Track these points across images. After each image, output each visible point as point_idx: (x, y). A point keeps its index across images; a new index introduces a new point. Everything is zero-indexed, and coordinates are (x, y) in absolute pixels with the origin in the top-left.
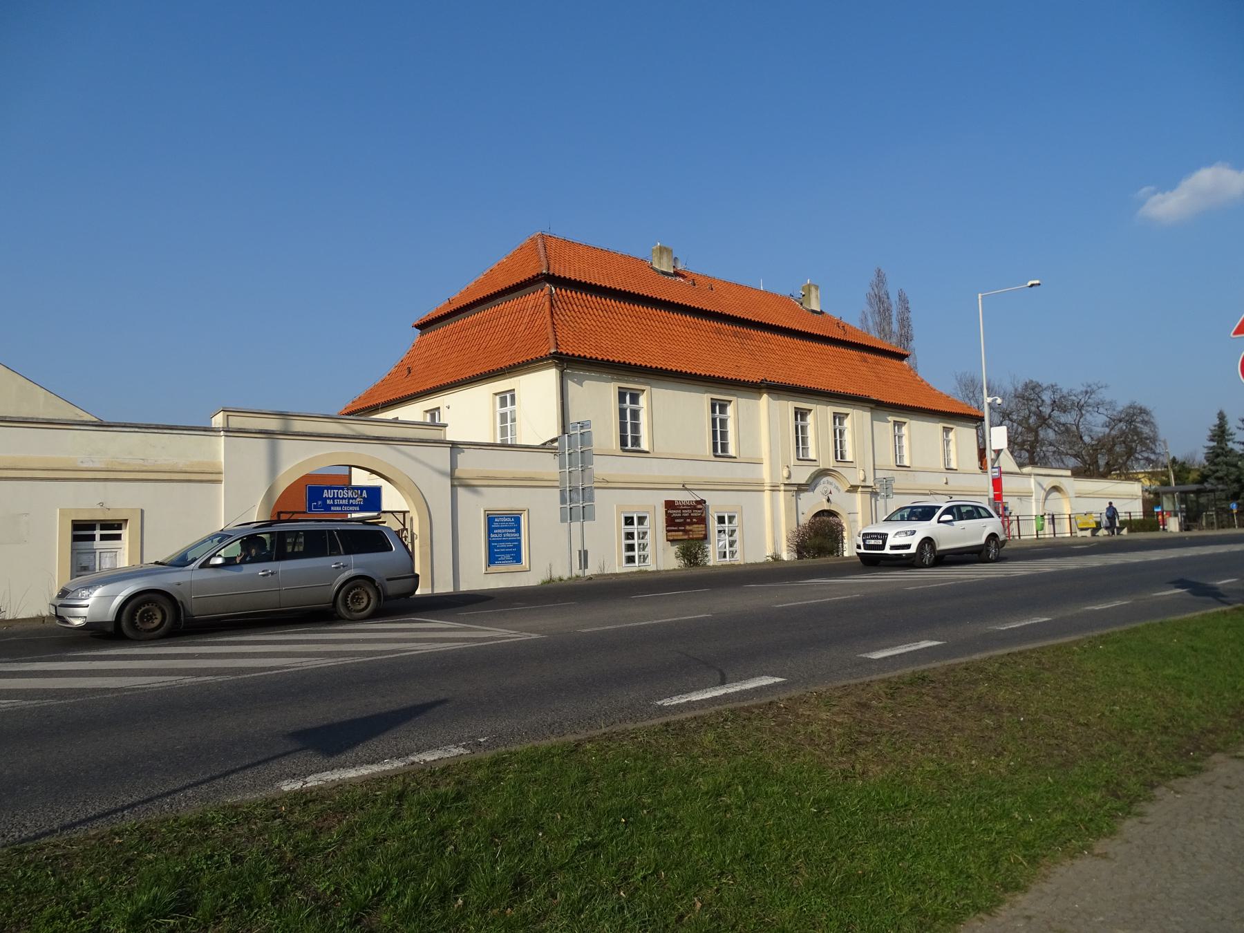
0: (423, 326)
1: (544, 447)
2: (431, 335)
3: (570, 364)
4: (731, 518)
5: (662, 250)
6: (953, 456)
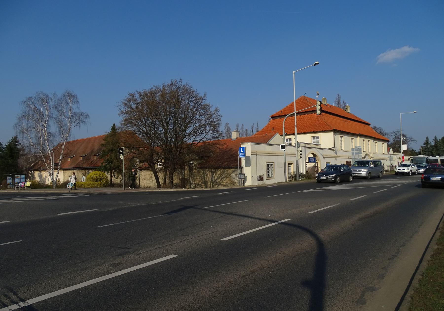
0: (273, 117)
1: (330, 149)
2: (276, 120)
3: (336, 131)
4: (271, 165)
5: (325, 99)
6: (343, 146)
